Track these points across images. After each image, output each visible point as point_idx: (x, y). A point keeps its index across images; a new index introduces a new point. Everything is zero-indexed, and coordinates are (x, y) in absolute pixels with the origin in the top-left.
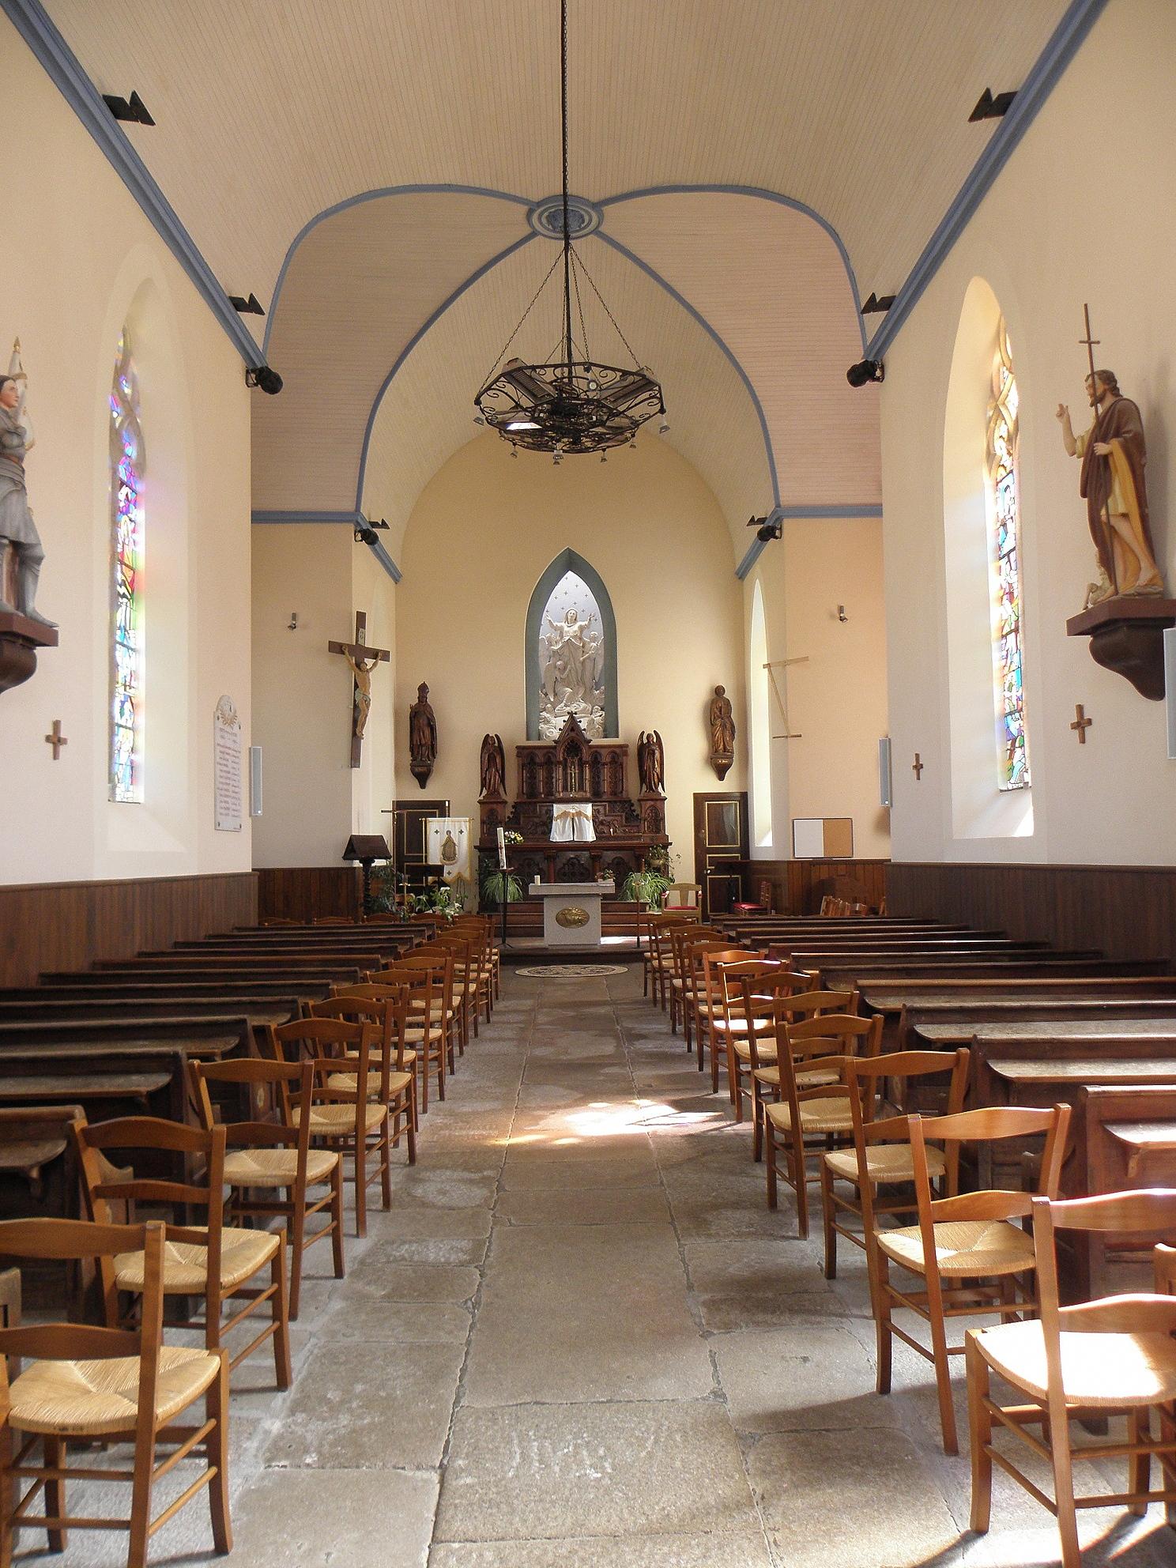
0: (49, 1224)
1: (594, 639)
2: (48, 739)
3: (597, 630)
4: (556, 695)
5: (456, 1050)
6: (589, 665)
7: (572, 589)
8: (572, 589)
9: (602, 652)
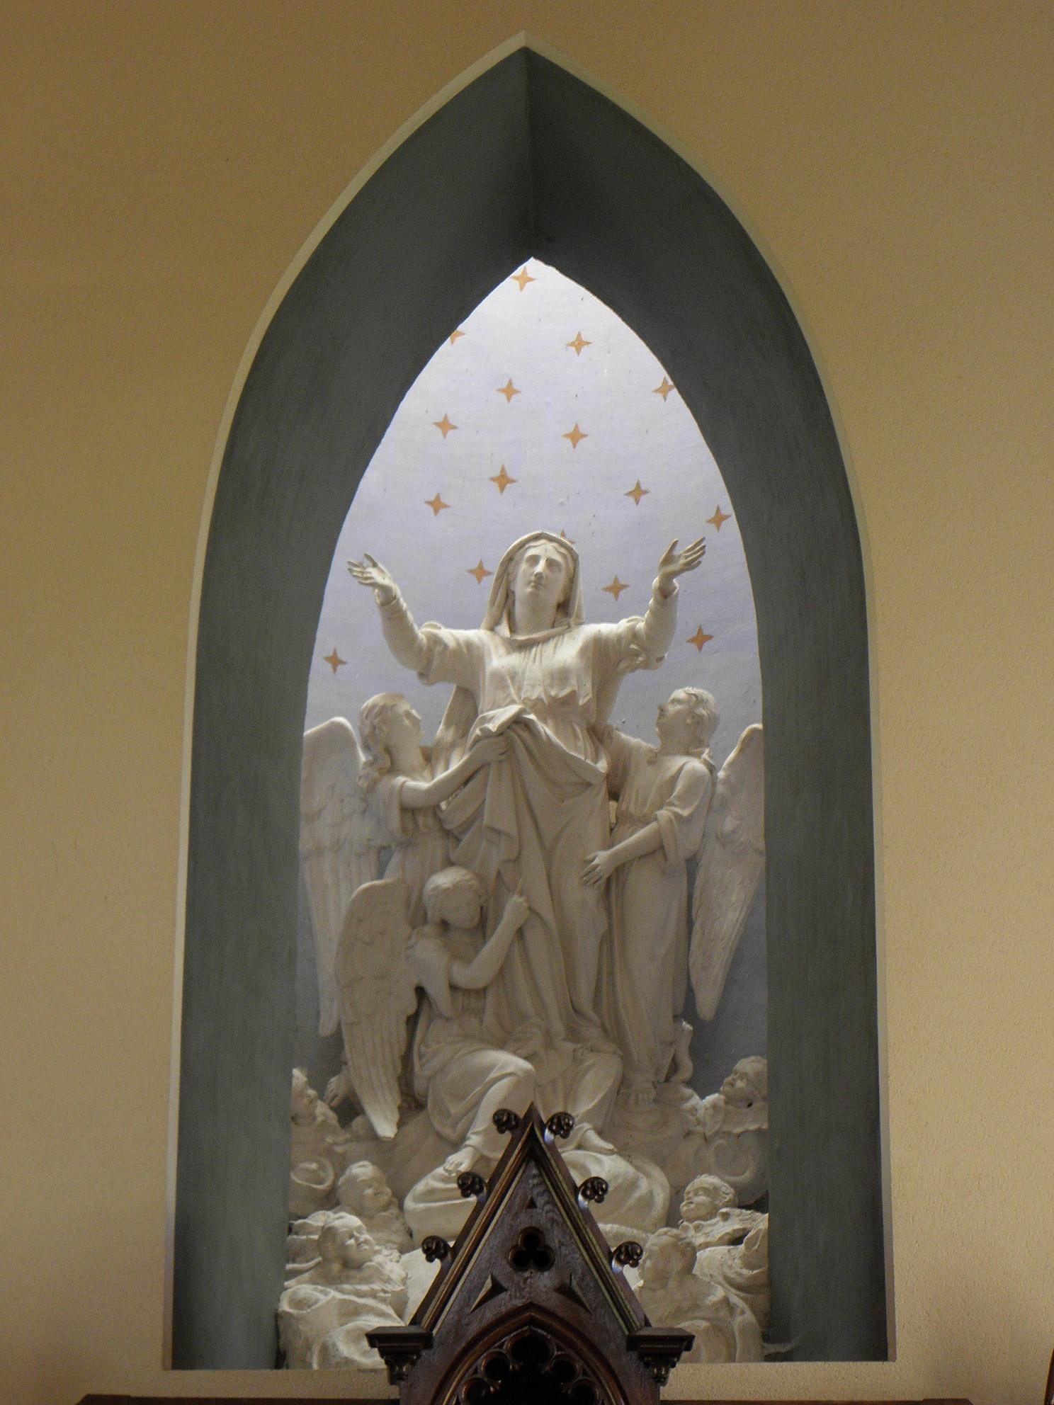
0: (405, 600)
1: (691, 730)
2: (578, 351)
3: (722, 675)
4: (412, 1104)
5: (562, 550)
6: (652, 901)
7: (543, 391)
8: (543, 391)
9: (744, 822)
